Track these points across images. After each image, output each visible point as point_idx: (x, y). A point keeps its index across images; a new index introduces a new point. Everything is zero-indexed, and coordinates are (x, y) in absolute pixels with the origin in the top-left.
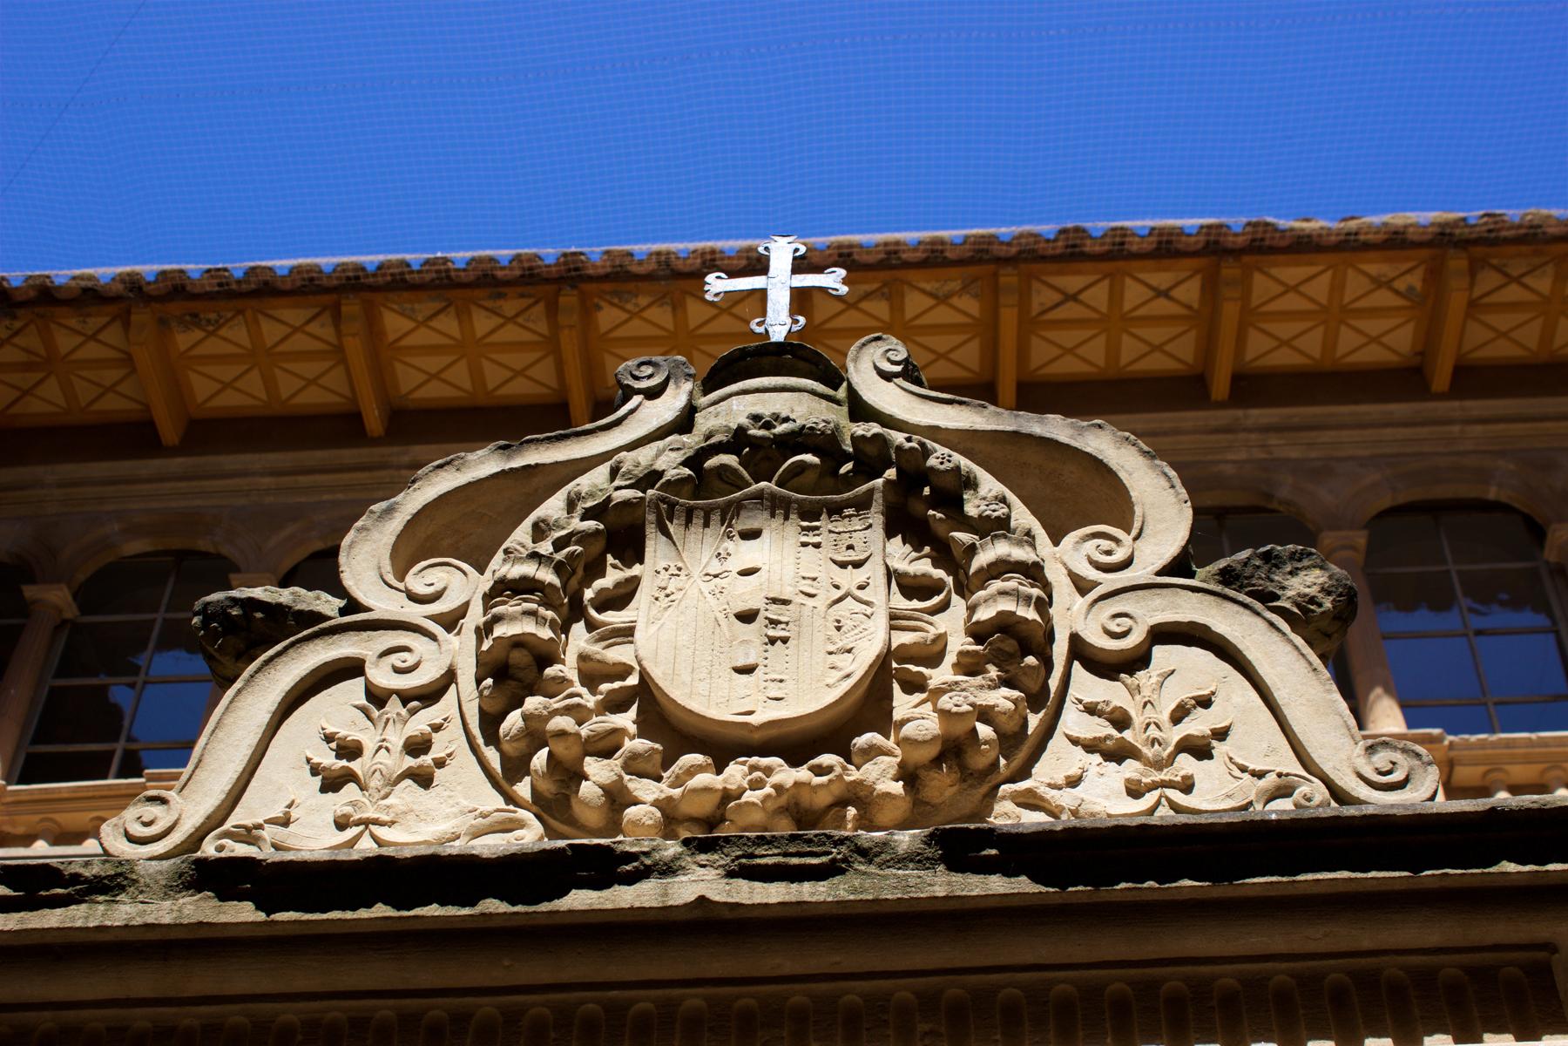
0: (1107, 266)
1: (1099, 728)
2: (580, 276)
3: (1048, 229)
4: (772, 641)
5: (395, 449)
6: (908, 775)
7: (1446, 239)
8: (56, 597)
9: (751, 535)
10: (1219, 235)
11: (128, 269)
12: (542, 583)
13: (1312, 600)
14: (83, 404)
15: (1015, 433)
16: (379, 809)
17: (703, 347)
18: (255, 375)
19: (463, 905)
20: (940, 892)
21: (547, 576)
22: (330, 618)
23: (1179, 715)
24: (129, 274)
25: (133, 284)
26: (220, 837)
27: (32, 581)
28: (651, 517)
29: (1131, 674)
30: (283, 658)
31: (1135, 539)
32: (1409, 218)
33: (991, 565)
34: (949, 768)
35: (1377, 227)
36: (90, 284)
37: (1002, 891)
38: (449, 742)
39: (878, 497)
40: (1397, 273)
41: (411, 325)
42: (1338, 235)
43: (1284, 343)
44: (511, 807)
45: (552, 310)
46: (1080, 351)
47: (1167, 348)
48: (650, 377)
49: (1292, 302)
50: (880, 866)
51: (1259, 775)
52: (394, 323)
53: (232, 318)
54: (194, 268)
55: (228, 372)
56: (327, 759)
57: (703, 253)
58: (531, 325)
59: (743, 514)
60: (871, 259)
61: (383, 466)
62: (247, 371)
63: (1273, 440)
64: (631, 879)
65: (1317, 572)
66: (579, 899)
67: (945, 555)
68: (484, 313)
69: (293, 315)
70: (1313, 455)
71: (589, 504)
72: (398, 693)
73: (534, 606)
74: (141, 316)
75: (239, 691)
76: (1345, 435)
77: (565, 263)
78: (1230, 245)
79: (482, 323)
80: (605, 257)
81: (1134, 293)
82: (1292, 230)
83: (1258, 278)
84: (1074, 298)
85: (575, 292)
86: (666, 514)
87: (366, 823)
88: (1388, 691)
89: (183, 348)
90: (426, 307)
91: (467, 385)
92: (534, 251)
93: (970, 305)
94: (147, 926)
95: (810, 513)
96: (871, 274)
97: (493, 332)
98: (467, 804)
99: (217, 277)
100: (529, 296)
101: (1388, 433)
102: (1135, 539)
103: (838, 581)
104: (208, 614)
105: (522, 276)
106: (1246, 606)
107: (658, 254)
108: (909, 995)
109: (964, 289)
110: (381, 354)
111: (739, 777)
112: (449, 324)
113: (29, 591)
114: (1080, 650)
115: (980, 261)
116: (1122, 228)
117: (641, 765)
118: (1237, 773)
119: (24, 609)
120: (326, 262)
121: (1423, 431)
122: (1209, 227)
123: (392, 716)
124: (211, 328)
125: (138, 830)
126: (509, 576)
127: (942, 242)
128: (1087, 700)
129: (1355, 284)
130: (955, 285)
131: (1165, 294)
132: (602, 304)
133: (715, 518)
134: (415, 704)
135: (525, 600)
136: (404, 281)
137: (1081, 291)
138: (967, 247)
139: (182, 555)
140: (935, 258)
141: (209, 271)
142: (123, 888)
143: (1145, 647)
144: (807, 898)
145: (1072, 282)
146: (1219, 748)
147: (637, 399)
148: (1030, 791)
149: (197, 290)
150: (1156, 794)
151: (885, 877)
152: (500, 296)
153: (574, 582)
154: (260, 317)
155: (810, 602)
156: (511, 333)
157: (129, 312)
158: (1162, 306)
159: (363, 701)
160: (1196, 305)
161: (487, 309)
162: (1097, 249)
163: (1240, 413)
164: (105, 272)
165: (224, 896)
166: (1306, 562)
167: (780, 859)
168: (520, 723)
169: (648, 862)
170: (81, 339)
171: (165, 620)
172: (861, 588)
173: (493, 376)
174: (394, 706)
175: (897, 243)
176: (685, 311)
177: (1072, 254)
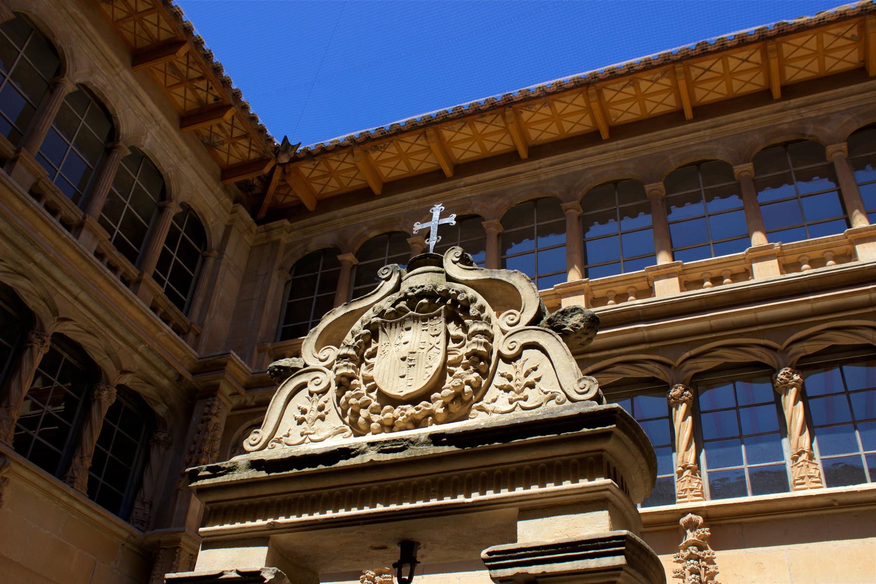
0: (720, 54)
1: (505, 382)
2: (511, 103)
3: (691, 45)
4: (410, 366)
5: (458, 180)
6: (446, 406)
7: (864, 12)
8: (349, 258)
9: (408, 329)
10: (763, 32)
11: (349, 135)
12: (349, 355)
13: (577, 325)
14: (346, 185)
15: (490, 279)
16: (311, 430)
17: (565, 119)
18: (402, 163)
19: (314, 467)
20: (431, 452)
21: (352, 352)
22: (301, 369)
23: (527, 374)
24: (349, 137)
25: (352, 140)
26: (272, 442)
27: (340, 253)
28: (380, 328)
29: (515, 362)
30: (287, 384)
31: (521, 313)
32: (846, 7)
33: (473, 332)
34: (456, 402)
35: (832, 14)
36: (337, 143)
37: (447, 451)
38: (330, 406)
39: (443, 312)
40: (845, 31)
41: (454, 133)
42: (815, 21)
43: (801, 69)
44: (345, 425)
45: (504, 117)
46: (716, 90)
47: (752, 81)
48: (387, 273)
49: (801, 52)
50: (417, 446)
51: (546, 393)
52: (447, 134)
53: (389, 144)
54: (371, 129)
55: (392, 164)
56: (299, 415)
57: (556, 84)
58: (498, 124)
59: (406, 323)
60: (623, 72)
61: (455, 188)
62: (399, 162)
63: (803, 111)
64: (354, 456)
65: (580, 315)
66: (342, 463)
67: (465, 329)
68: (479, 123)
69: (410, 139)
70: (821, 113)
71: (366, 324)
72: (316, 392)
73: (346, 363)
74: (357, 151)
75: (276, 396)
76: (833, 103)
77: (505, 99)
78: (769, 35)
79: (479, 127)
80: (519, 93)
81: (733, 63)
82: (794, 23)
83: (784, 46)
84: (708, 70)
85: (511, 109)
86: (384, 325)
87: (307, 434)
88: (861, 212)
89: (375, 159)
90: (457, 126)
91: (480, 151)
92: (492, 96)
93: (667, 81)
94: (241, 480)
95: (424, 320)
96: (624, 78)
97: (484, 130)
98: (333, 425)
99: (380, 131)
100: (495, 114)
101: (852, 98)
102: (521, 313)
103: (431, 342)
104: (272, 370)
105: (490, 107)
106: (551, 334)
107: (539, 88)
108: (429, 480)
109: (663, 76)
110: (445, 148)
111: (397, 413)
112: (467, 130)
113: (340, 257)
114: (500, 355)
115: (666, 64)
116: (722, 38)
117: (374, 411)
118: (541, 392)
119: (339, 264)
120: (417, 117)
121: (868, 94)
122: (759, 30)
123: (314, 399)
124: (382, 150)
125: (253, 442)
126: (341, 354)
127: (649, 60)
128: (501, 372)
129: (827, 39)
130: (659, 75)
131: (746, 60)
132: (523, 111)
133: (398, 325)
134: (320, 395)
135: (345, 361)
136: (447, 118)
137: (710, 67)
138: (660, 60)
139: (390, 234)
140: (648, 66)
141: (377, 130)
142: (235, 470)
143: (520, 351)
144: (397, 457)
145: (706, 64)
146: (538, 384)
147: (383, 282)
148: (480, 406)
149: (375, 137)
150: (516, 402)
151: (418, 449)
152: (483, 116)
153: (361, 351)
154: (399, 142)
155: (422, 351)
156: (491, 129)
157: (353, 150)
158: (746, 65)
159: (308, 396)
160: (760, 62)
161: (480, 122)
162: (713, 49)
163: (787, 102)
164: (341, 138)
165: (258, 470)
166: (576, 312)
167: (391, 447)
168: (345, 400)
169: (358, 451)
170: (339, 163)
171: (388, 259)
172: (438, 343)
173: (488, 146)
174: (315, 396)
175: (632, 64)
176: (555, 107)
177: (703, 53)
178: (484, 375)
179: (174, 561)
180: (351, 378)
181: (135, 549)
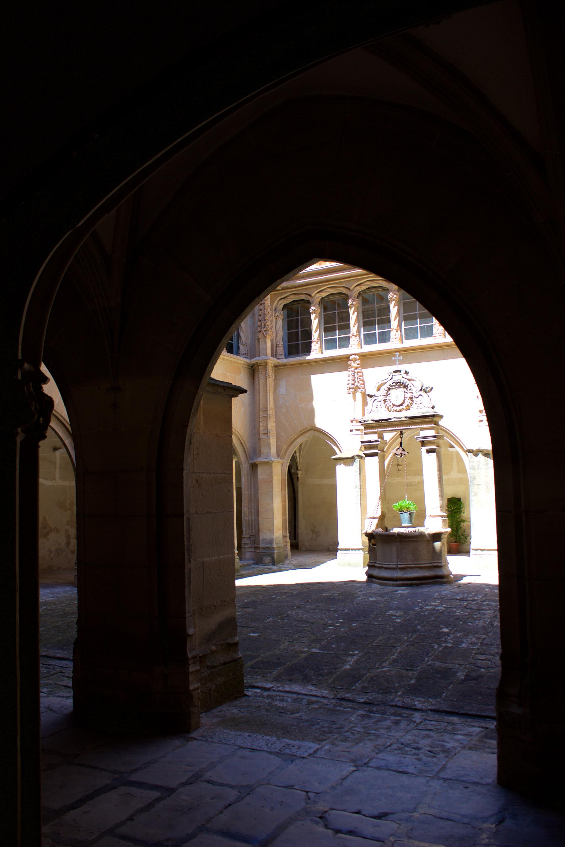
66: (389, 421)
178: (412, 401)
179: (267, 371)
180: (386, 400)
181: (247, 367)
